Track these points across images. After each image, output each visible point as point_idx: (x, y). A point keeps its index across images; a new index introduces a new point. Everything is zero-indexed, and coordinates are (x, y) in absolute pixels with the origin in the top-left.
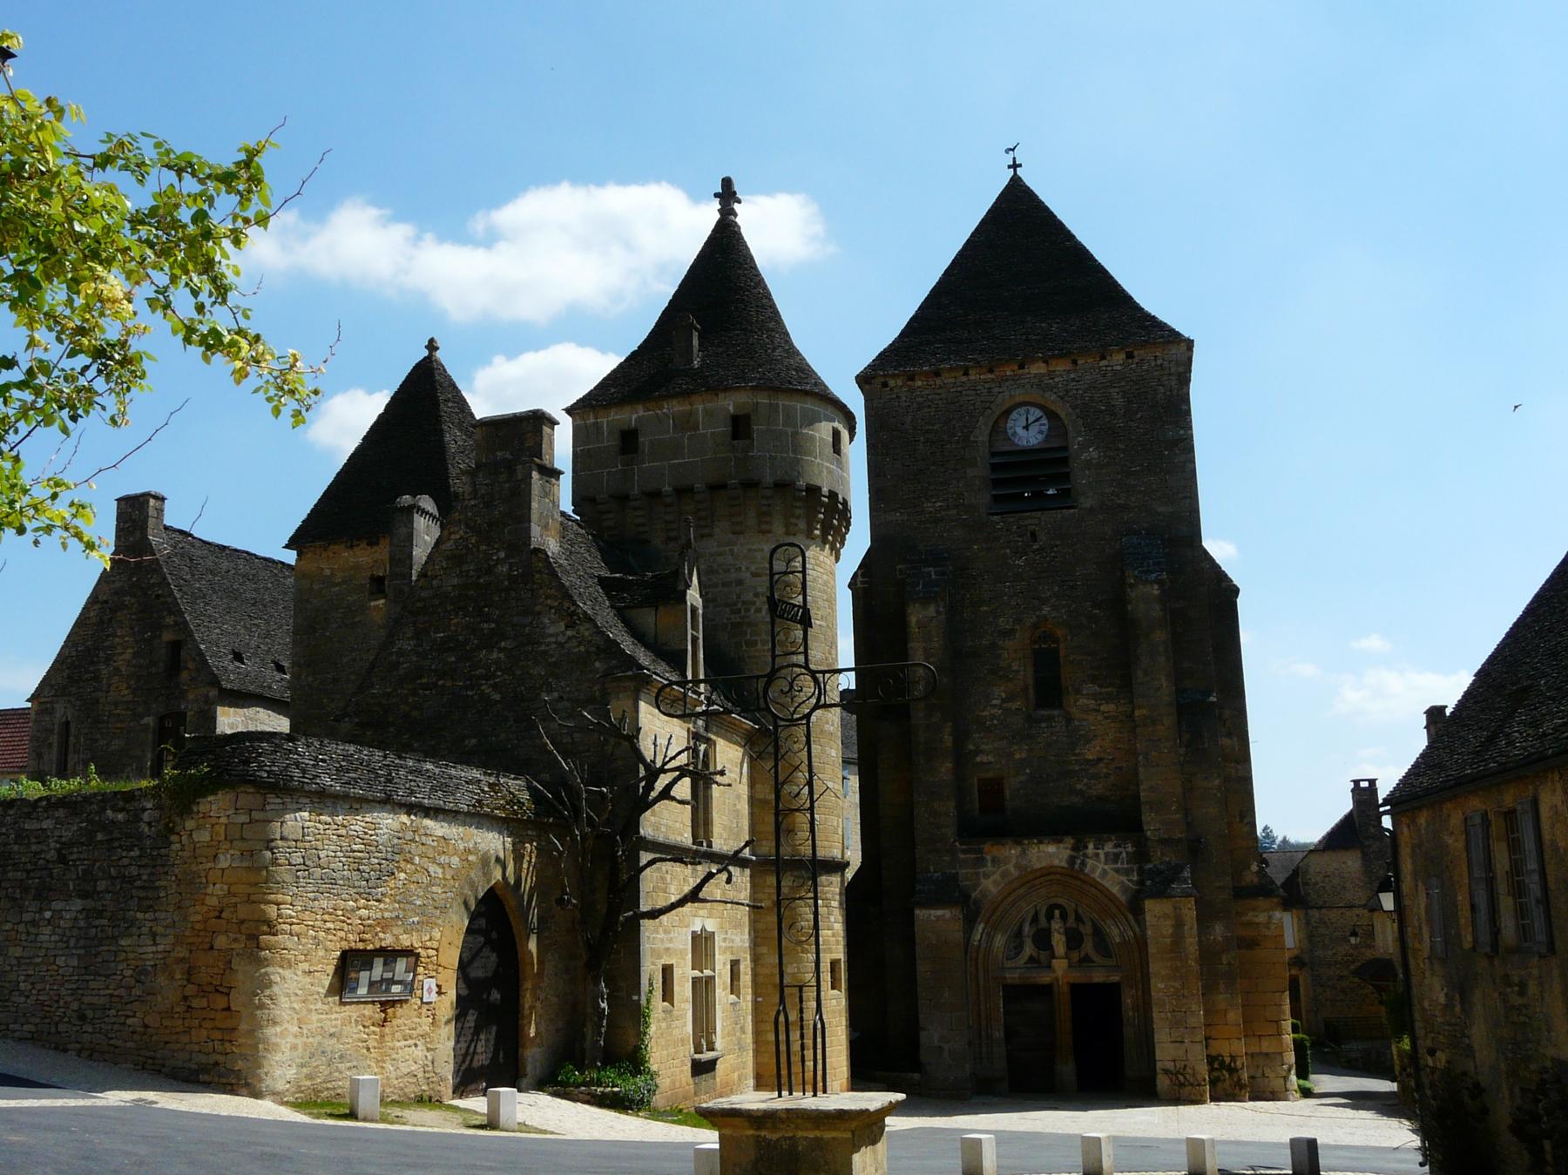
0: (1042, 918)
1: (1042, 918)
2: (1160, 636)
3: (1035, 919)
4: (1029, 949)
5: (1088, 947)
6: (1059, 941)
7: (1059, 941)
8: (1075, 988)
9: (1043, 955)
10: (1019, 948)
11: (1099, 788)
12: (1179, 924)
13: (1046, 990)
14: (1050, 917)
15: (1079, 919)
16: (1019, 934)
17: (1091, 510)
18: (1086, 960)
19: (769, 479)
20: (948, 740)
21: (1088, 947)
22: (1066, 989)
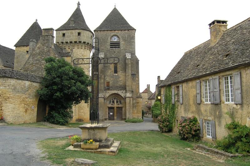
0: (113, 99)
1: (113, 99)
2: (130, 65)
3: (113, 99)
4: (112, 103)
5: (119, 103)
6: (115, 102)
7: (115, 102)
8: (117, 108)
9: (113, 104)
10: (110, 103)
11: (121, 84)
12: (130, 100)
13: (113, 108)
14: (114, 99)
15: (118, 99)
16: (110, 101)
17: (122, 49)
18: (118, 104)
19: (82, 41)
20: (103, 77)
21: (119, 103)
22: (116, 108)
